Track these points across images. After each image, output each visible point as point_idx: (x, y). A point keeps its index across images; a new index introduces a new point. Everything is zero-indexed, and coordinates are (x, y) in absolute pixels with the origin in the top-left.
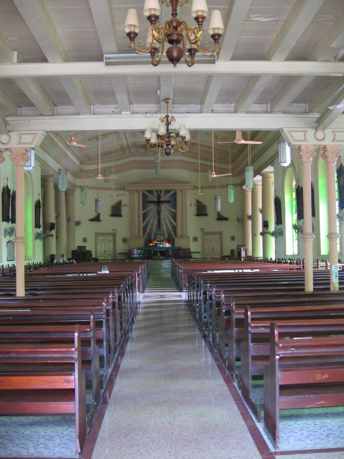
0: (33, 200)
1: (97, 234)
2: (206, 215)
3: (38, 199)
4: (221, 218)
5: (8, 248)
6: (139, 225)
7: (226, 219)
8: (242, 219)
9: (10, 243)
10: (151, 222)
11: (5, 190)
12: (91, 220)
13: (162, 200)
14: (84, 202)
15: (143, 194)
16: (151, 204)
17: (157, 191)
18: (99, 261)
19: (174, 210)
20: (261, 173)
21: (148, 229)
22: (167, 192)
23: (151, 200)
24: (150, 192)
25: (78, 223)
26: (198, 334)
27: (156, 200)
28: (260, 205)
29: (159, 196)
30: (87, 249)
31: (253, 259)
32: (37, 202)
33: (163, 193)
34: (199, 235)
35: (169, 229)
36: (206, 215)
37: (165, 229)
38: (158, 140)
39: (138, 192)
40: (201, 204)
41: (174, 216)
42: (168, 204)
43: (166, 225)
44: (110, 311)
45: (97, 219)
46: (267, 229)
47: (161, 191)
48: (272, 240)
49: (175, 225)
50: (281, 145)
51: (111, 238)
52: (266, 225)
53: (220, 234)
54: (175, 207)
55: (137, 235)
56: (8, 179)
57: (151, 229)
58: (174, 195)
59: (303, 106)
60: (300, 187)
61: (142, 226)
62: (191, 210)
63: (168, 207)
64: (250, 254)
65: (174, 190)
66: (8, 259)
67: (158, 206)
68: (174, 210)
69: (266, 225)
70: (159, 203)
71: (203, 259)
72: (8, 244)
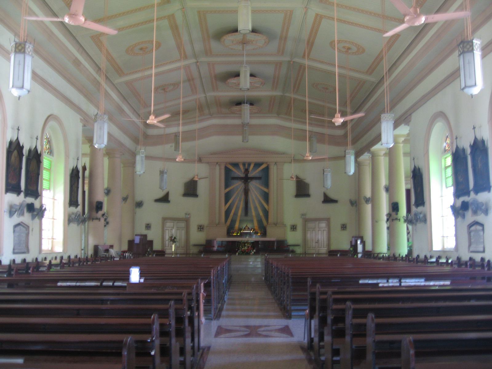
0: (66, 167)
1: (165, 220)
2: (308, 195)
3: (75, 166)
4: (327, 200)
5: (17, 234)
6: (220, 207)
7: (335, 201)
8: (356, 202)
9: (20, 226)
10: (236, 204)
11: (13, 147)
12: (157, 201)
13: (250, 175)
14: (163, 188)
17: (244, 164)
18: (166, 256)
19: (266, 190)
20: (370, 150)
21: (232, 214)
22: (257, 165)
23: (236, 176)
24: (236, 165)
25: (139, 204)
27: (242, 175)
28: (383, 181)
29: (247, 171)
30: (149, 238)
31: (376, 255)
32: (73, 170)
34: (299, 223)
35: (259, 214)
36: (308, 195)
37: (254, 214)
39: (220, 165)
41: (266, 197)
42: (258, 181)
43: (256, 208)
45: (165, 199)
46: (397, 214)
47: (249, 164)
48: (403, 228)
49: (267, 209)
51: (183, 225)
52: (395, 207)
53: (328, 220)
54: (267, 184)
55: (217, 222)
56: (18, 130)
57: (236, 214)
58: (267, 170)
60: (417, 167)
61: (224, 209)
62: (290, 188)
63: (258, 185)
64: (369, 248)
65: (267, 163)
66: (16, 251)
67: (245, 184)
68: (266, 190)
69: (395, 207)
70: (246, 179)
71: (304, 255)
72: (18, 229)
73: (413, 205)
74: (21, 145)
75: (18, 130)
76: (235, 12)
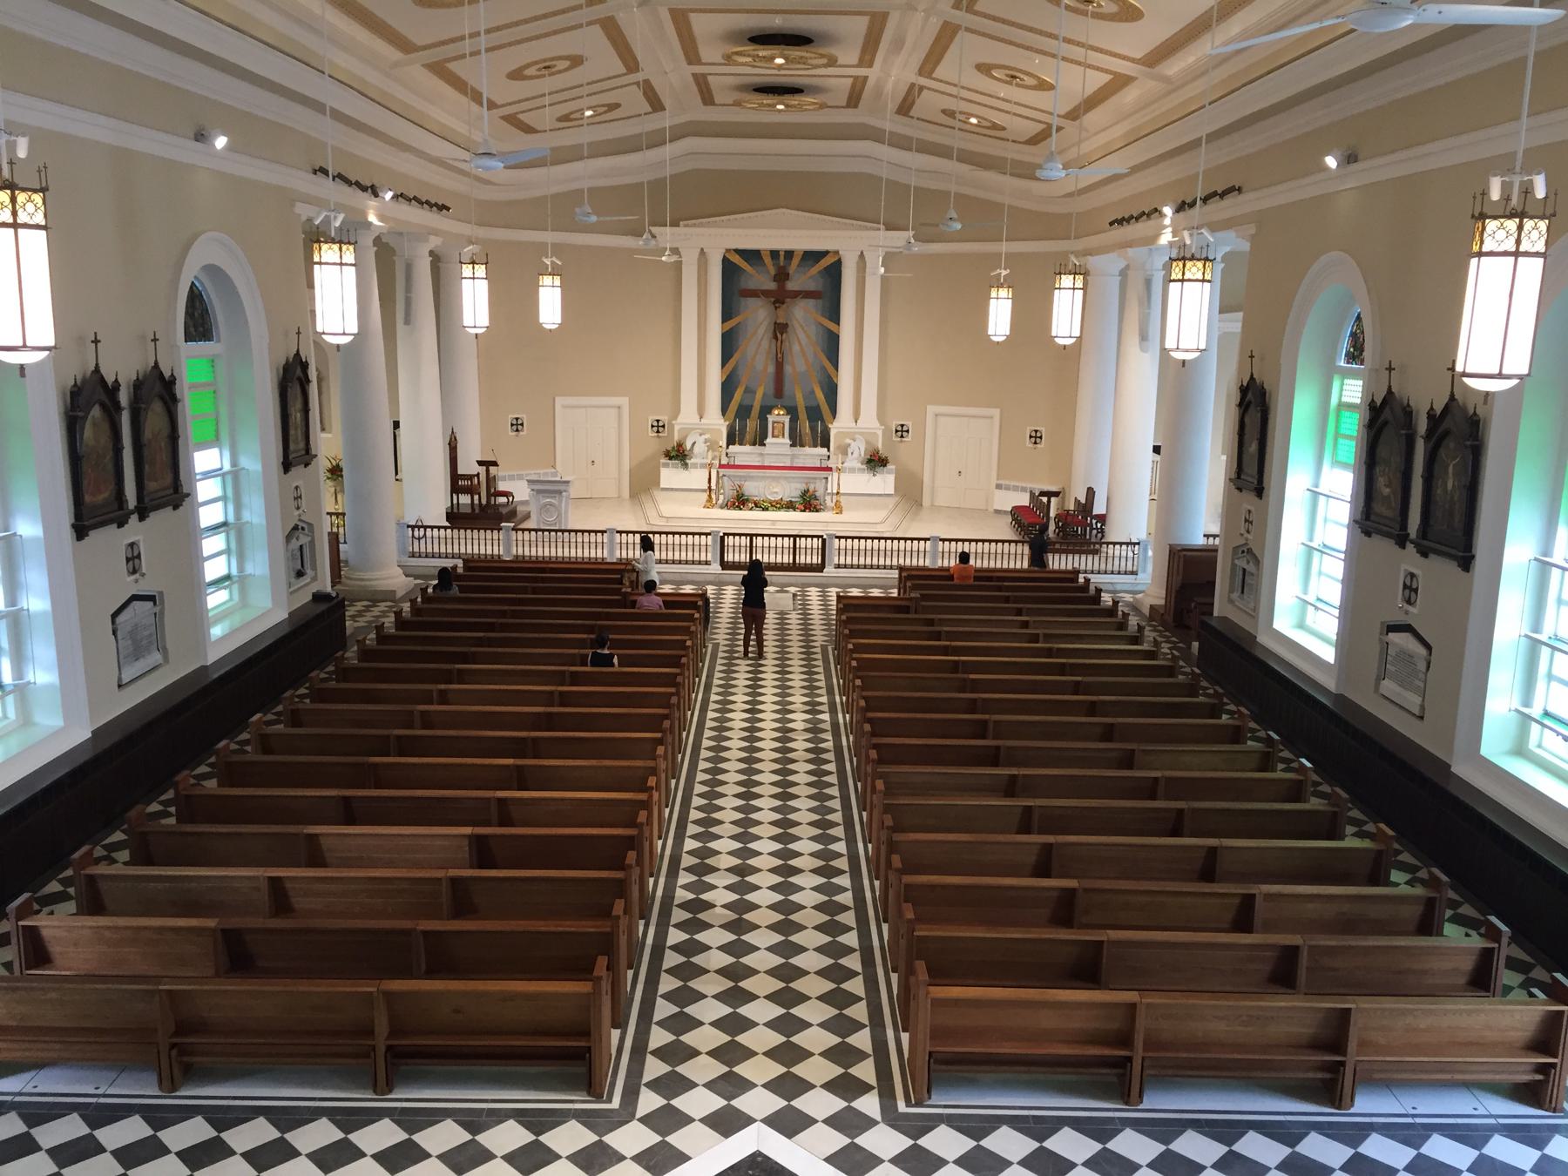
15: (725, 261)
16: (752, 302)
17: (774, 254)
22: (812, 257)
26: (835, 725)
27: (772, 286)
29: (782, 276)
33: (796, 261)
38: (695, 466)
40: (1216, 7)
44: (1513, 955)
47: (789, 254)
50: (119, 1081)
59: (814, 502)
68: (831, 326)
70: (780, 297)
73: (1422, 437)
74: (167, 374)
75: (299, 333)
76: (219, 341)
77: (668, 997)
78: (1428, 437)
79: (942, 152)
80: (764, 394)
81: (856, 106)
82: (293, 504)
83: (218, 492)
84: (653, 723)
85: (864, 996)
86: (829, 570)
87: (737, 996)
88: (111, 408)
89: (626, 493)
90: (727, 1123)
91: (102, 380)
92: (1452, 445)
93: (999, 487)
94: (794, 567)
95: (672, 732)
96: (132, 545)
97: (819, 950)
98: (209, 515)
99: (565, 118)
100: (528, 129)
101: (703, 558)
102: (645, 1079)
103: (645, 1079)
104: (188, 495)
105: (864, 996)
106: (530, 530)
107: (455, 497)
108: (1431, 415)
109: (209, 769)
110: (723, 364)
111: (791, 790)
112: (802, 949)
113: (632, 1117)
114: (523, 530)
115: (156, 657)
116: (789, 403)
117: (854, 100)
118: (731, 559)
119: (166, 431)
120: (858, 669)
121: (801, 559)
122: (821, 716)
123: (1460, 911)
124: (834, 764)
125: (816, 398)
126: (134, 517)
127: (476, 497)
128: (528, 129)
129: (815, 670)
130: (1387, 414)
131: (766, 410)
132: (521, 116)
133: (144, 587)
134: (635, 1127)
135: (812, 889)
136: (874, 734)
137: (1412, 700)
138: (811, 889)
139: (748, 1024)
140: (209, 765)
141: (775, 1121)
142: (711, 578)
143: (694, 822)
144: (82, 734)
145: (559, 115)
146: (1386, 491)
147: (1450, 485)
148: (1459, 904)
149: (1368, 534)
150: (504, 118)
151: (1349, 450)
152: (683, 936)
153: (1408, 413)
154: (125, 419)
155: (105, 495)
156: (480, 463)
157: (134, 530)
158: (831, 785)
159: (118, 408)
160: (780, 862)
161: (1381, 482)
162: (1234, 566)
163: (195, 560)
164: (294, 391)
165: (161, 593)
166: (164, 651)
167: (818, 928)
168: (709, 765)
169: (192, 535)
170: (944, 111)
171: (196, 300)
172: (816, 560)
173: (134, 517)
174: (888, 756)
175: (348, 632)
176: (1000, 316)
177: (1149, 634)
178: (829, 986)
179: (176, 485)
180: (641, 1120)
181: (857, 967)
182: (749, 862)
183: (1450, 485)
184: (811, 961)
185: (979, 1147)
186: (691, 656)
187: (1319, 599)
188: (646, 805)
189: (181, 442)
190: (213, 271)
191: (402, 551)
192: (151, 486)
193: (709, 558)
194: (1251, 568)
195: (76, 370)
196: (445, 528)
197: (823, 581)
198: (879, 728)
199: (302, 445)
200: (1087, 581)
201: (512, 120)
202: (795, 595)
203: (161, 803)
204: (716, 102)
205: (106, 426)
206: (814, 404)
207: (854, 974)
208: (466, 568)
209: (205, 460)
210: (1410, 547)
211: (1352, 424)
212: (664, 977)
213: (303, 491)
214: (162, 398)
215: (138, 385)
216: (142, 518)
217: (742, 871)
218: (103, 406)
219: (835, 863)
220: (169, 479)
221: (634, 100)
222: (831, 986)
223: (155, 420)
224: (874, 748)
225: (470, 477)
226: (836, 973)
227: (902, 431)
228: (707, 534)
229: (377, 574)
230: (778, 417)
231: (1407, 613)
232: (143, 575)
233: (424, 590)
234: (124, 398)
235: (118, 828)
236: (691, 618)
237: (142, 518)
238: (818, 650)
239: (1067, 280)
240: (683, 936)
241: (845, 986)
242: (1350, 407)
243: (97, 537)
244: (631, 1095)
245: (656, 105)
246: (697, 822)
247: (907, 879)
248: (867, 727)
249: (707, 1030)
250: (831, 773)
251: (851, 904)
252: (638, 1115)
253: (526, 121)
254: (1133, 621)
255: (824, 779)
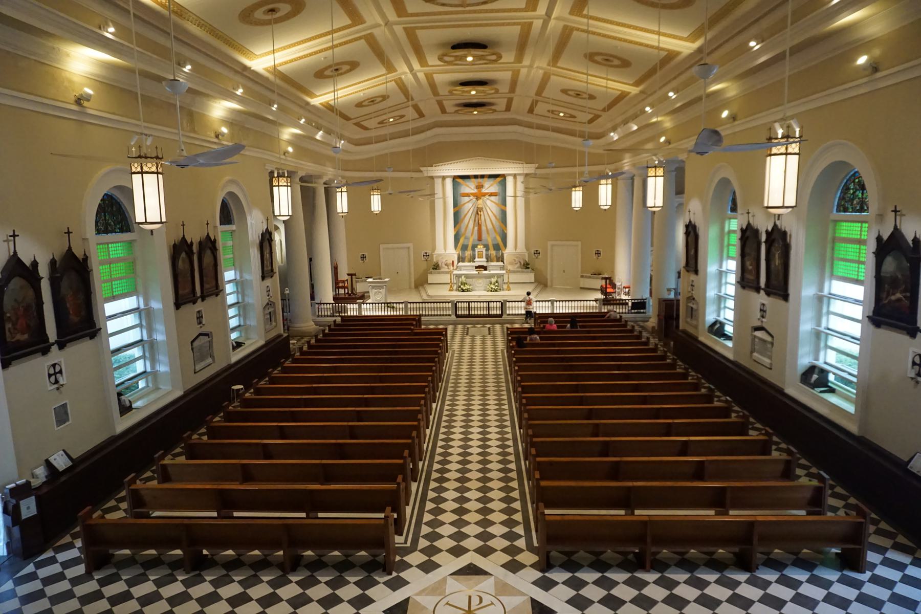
27: (475, 191)
77: (430, 512)
78: (766, 242)
79: (546, 128)
80: (473, 240)
81: (509, 110)
82: (266, 294)
83: (141, 354)
84: (421, 390)
85: (523, 535)
86: (504, 317)
87: (461, 511)
88: (190, 254)
89: (413, 285)
90: (458, 551)
91: (186, 241)
92: (777, 245)
93: (582, 276)
94: (489, 316)
95: (429, 393)
96: (199, 312)
97: (500, 489)
98: (231, 299)
99: (381, 123)
100: (366, 128)
101: (448, 313)
102: (422, 534)
103: (422, 534)
104: (222, 290)
105: (520, 509)
106: (370, 303)
107: (337, 290)
108: (767, 231)
109: (219, 419)
110: (455, 227)
111: (487, 424)
112: (492, 489)
113: (415, 550)
114: (367, 304)
115: (209, 360)
116: (485, 243)
117: (508, 108)
118: (460, 313)
119: (213, 262)
120: (516, 362)
121: (492, 312)
122: (501, 384)
123: (780, 446)
124: (509, 422)
125: (497, 240)
126: (200, 300)
127: (346, 290)
128: (366, 128)
129: (501, 388)
130: (748, 233)
131: (474, 247)
132: (362, 123)
133: (205, 330)
134: (417, 554)
135: (497, 470)
136: (529, 419)
137: (766, 361)
138: (497, 470)
139: (467, 511)
140: (220, 417)
141: (479, 551)
142: (451, 322)
143: (439, 454)
144: (179, 393)
145: (379, 121)
146: (750, 268)
147: (777, 263)
148: (779, 443)
149: (743, 287)
150: (355, 124)
151: (734, 251)
152: (440, 466)
153: (756, 232)
154: (195, 258)
155: (188, 290)
156: (348, 275)
157: (199, 306)
158: (506, 421)
159: (192, 253)
160: (482, 443)
161: (748, 263)
162: (687, 306)
163: (226, 319)
164: (266, 244)
165: (211, 333)
166: (213, 357)
167: (501, 511)
168: (445, 430)
169: (225, 307)
170: (549, 111)
171: (225, 207)
172: (499, 312)
173: (200, 300)
174: (525, 389)
175: (291, 350)
176: (577, 198)
177: (652, 340)
178: (506, 530)
179: (217, 286)
180: (419, 551)
181: (522, 532)
182: (468, 443)
183: (777, 263)
184: (496, 505)
185: (578, 594)
186: (438, 365)
187: (725, 319)
188: (417, 428)
189: (218, 267)
190: (231, 194)
191: (314, 314)
192: (206, 286)
193: (450, 313)
194: (694, 307)
195: (176, 237)
196: (333, 304)
197: (502, 321)
198: (525, 389)
199: (270, 268)
200: (621, 317)
201: (358, 124)
202: (489, 328)
203: (198, 434)
204: (448, 111)
205: (187, 261)
206: (496, 243)
207: (520, 536)
208: (342, 320)
209: (229, 275)
210: (762, 292)
211: (735, 239)
212: (423, 527)
213: (270, 288)
214: (210, 249)
215: (200, 243)
216: (203, 300)
217: (464, 462)
218: (187, 253)
219: (507, 443)
220: (214, 283)
221: (410, 113)
222: (506, 517)
223: (208, 258)
224: (526, 412)
225: (344, 282)
226: (508, 500)
227: (537, 253)
228: (449, 302)
229: (303, 325)
230: (480, 248)
231: (762, 322)
232: (203, 325)
233: (324, 331)
234: (195, 248)
235: (195, 433)
236: (440, 340)
237: (203, 300)
238: (500, 352)
239: (603, 181)
240: (437, 485)
241: (515, 543)
242: (734, 232)
243: (184, 309)
244: (415, 541)
245: (421, 115)
246: (437, 471)
247: (538, 459)
248: (519, 378)
249: (446, 540)
250: (506, 415)
251: (513, 452)
252: (419, 548)
253: (365, 125)
254: (645, 334)
255: (502, 407)
